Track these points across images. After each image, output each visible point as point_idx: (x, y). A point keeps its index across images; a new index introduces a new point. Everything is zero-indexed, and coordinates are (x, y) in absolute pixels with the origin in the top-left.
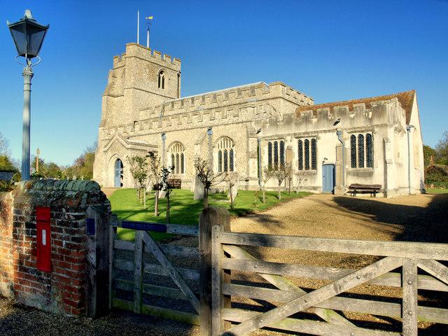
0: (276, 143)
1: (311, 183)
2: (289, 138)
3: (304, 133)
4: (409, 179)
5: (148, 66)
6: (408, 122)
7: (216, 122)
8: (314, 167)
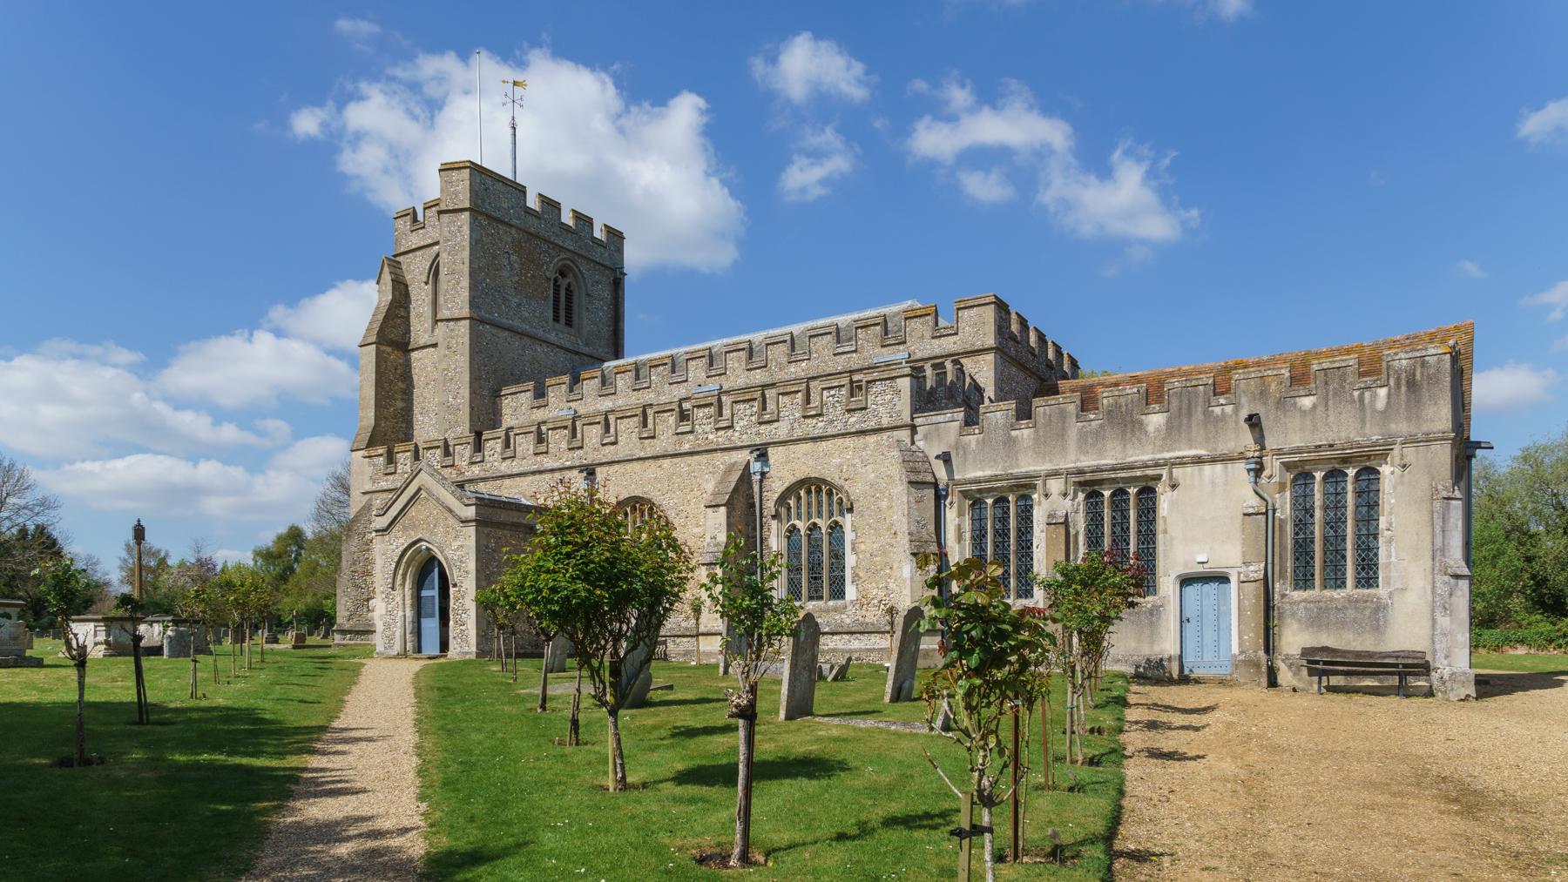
7: (782, 430)
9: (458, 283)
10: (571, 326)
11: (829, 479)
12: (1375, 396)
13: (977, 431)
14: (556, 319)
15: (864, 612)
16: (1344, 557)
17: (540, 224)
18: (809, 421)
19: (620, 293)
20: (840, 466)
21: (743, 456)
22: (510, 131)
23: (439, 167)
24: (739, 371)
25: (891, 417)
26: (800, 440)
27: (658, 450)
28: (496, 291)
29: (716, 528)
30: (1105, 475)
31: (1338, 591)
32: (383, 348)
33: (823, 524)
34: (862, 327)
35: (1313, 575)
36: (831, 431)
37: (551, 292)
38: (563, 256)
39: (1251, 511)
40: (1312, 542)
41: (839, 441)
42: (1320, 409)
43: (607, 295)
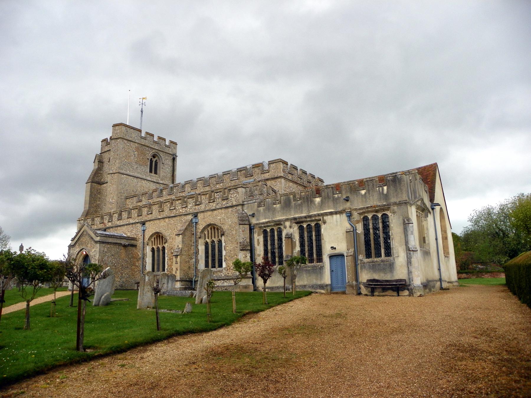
0: (272, 231)
1: (317, 279)
2: (288, 224)
3: (305, 217)
4: (439, 269)
5: (137, 149)
6: (432, 199)
7: (202, 207)
8: (320, 259)
9: (116, 162)
10: (156, 174)
11: (217, 224)
12: (383, 189)
13: (263, 206)
14: (151, 171)
15: (228, 272)
16: (380, 246)
17: (146, 141)
18: (210, 204)
19: (175, 162)
20: (220, 219)
21: (190, 217)
22: (141, 113)
23: (112, 125)
24: (201, 187)
25: (236, 202)
26: (208, 211)
27: (165, 216)
28: (129, 163)
29: (179, 243)
30: (303, 220)
31: (379, 258)
32: (93, 184)
33: (216, 240)
34: (239, 171)
35: (371, 253)
36: (218, 207)
37: (149, 163)
38: (154, 151)
39: (348, 231)
40: (370, 241)
41: (220, 211)
42: (367, 194)
43: (170, 163)
